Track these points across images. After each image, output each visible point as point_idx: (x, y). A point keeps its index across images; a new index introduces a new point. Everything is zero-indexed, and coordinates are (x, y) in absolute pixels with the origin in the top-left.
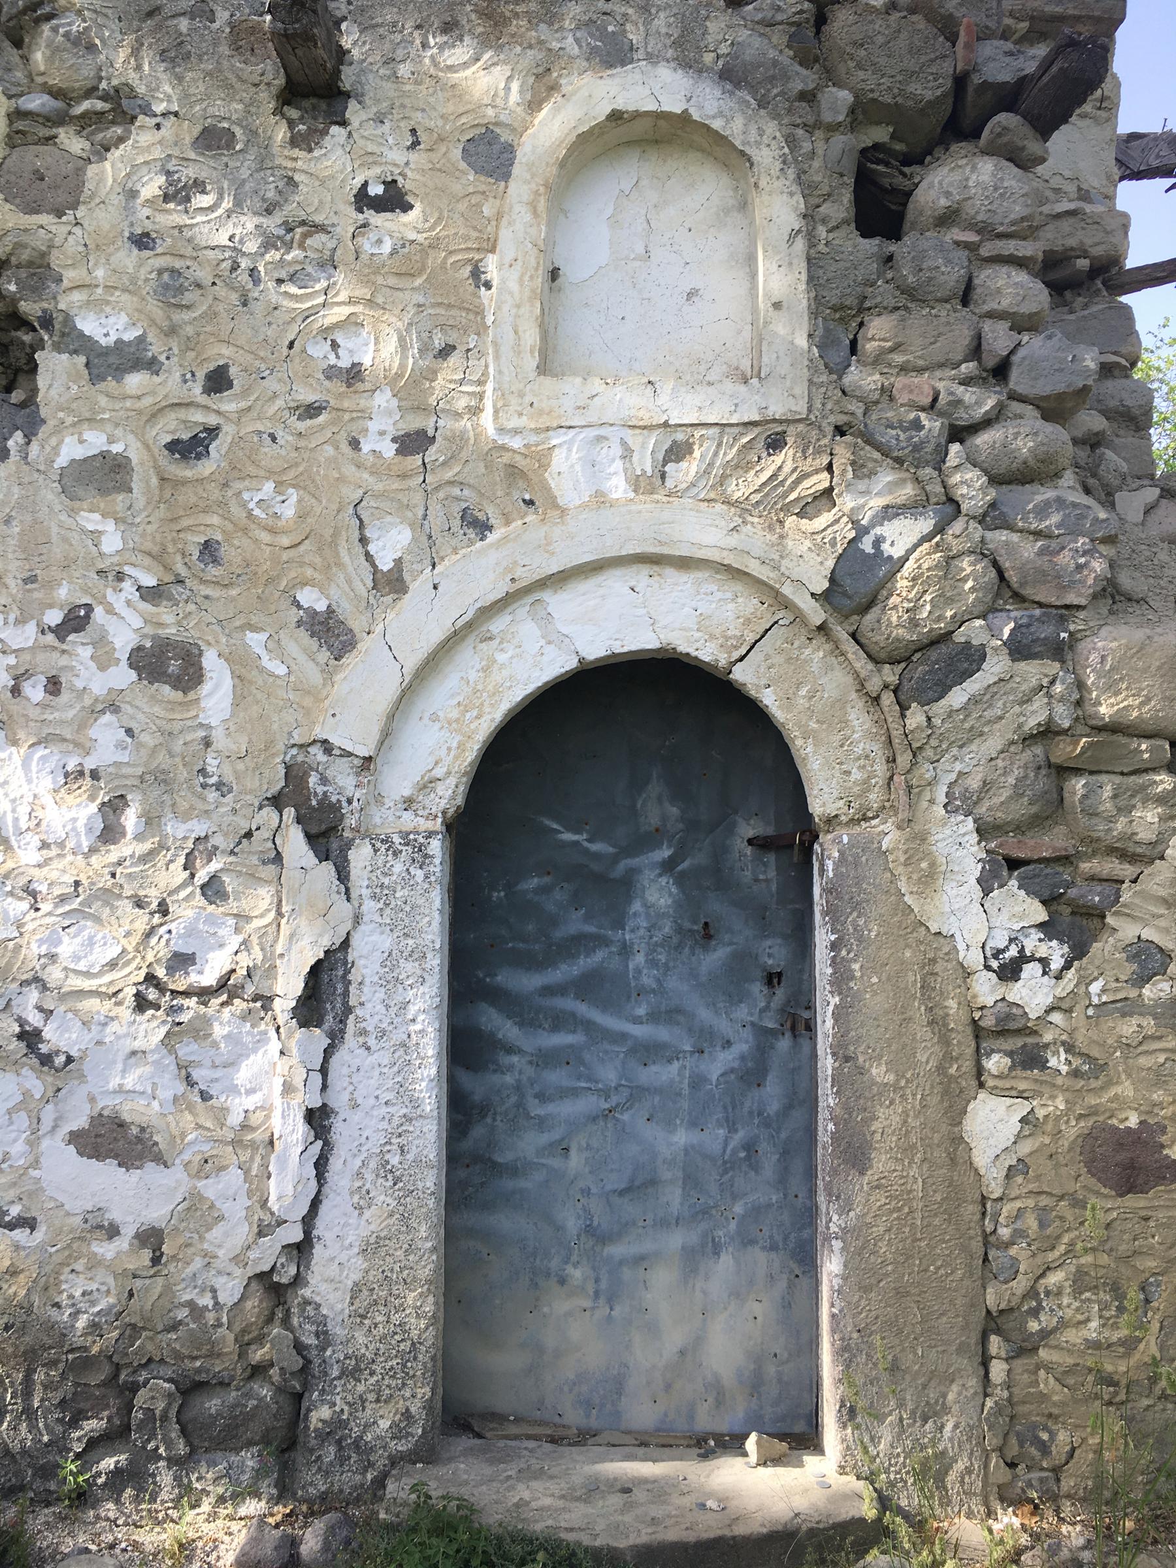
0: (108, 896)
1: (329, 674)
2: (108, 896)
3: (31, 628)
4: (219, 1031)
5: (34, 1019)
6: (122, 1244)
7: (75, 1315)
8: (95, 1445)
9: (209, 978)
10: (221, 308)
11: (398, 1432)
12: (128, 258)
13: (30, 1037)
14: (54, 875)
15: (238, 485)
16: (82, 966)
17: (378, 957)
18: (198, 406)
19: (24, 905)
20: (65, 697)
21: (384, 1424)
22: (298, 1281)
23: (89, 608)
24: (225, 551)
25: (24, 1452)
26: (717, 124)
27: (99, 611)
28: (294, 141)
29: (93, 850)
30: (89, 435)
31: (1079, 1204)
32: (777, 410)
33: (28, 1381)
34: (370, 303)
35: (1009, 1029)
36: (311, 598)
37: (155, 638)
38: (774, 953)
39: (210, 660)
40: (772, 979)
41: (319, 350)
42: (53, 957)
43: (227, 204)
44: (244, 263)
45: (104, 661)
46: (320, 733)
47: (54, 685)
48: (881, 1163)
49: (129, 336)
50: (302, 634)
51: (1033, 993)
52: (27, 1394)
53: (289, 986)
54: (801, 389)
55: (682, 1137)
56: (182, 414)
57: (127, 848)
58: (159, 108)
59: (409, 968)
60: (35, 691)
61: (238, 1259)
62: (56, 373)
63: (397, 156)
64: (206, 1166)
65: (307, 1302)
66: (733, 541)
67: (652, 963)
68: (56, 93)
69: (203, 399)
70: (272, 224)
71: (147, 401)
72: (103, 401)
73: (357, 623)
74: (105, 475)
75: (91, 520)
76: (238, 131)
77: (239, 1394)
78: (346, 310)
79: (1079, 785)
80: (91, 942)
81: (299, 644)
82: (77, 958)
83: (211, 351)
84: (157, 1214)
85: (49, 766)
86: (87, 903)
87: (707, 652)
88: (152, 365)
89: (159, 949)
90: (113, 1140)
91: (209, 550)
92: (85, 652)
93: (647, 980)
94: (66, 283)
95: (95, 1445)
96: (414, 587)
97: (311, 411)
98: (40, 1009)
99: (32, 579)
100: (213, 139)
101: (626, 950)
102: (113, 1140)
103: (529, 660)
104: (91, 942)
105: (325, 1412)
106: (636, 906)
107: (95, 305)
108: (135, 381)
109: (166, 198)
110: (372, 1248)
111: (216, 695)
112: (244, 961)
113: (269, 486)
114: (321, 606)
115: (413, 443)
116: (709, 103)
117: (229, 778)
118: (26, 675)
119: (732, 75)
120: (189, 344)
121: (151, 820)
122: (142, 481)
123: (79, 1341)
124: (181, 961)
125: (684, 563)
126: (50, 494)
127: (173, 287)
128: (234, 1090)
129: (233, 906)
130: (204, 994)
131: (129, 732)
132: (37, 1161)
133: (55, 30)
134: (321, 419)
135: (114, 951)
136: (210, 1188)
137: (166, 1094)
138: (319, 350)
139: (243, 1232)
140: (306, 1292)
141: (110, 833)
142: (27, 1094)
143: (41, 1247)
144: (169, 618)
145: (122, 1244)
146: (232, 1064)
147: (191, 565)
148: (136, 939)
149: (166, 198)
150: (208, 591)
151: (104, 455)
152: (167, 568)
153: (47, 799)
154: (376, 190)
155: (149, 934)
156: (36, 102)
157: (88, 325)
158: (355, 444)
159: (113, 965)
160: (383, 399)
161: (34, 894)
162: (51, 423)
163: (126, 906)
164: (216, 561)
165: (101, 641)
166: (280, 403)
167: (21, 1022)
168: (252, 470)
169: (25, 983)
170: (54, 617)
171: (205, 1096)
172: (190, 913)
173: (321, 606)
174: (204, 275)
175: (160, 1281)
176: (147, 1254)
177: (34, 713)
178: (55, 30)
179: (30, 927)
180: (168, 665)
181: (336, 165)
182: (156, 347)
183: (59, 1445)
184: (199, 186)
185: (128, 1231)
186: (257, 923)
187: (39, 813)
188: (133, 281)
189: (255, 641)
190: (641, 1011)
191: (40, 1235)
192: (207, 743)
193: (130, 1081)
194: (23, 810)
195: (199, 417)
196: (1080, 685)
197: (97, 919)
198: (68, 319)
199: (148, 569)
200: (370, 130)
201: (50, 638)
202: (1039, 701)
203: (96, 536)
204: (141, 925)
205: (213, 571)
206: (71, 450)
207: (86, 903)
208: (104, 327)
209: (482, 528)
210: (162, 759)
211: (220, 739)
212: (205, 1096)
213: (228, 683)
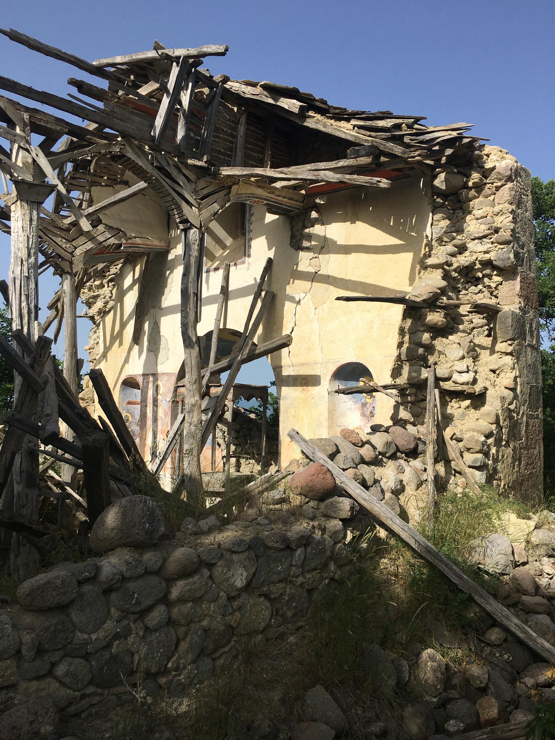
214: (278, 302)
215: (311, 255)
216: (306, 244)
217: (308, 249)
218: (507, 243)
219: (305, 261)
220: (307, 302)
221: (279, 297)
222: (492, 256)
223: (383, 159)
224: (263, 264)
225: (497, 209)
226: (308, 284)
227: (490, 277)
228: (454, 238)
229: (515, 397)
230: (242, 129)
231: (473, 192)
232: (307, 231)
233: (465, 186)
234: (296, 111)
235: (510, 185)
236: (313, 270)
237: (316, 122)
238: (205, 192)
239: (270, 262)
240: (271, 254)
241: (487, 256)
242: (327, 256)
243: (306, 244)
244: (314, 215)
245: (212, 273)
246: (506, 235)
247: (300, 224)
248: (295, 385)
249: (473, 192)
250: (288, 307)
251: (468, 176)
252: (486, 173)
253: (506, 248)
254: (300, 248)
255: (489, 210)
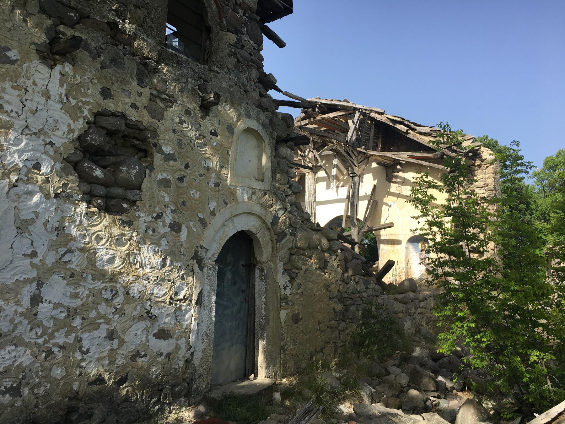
0: (163, 279)
1: (203, 231)
2: (163, 279)
3: (150, 217)
4: (183, 308)
5: (149, 308)
6: (163, 357)
7: (152, 376)
8: (155, 404)
9: (181, 297)
10: (188, 150)
11: (206, 387)
12: (172, 134)
13: (148, 312)
14: (153, 275)
15: (190, 189)
16: (158, 296)
17: (207, 291)
18: (182, 170)
19: (147, 282)
20: (156, 233)
21: (204, 386)
22: (192, 360)
23: (162, 214)
24: (187, 204)
25: (142, 410)
26: (261, 134)
27: (164, 214)
28: (201, 117)
29: (161, 269)
30: (163, 174)
31: (292, 327)
32: (266, 189)
33: (143, 392)
34: (212, 155)
35: (285, 299)
36: (201, 215)
37: (174, 222)
38: (244, 287)
39: (184, 227)
40: (243, 291)
41: (203, 162)
42: (153, 294)
43: (190, 127)
44: (193, 142)
45: (164, 226)
46: (201, 244)
47: (154, 231)
48: (271, 323)
49: (171, 152)
50: (199, 222)
51: (288, 292)
52: (142, 396)
53: (195, 298)
54: (269, 185)
55: (229, 324)
56: (180, 172)
57: (167, 268)
58: (179, 102)
59: (212, 293)
60: (150, 232)
61: (183, 357)
62: (158, 159)
63: (216, 125)
64: (178, 339)
65: (192, 364)
66: (260, 211)
67: (227, 290)
68: (158, 91)
69: (184, 169)
70: (197, 134)
71: (174, 168)
72: (166, 166)
73: (208, 221)
74: (165, 183)
75: (163, 193)
76: (192, 112)
77: (179, 386)
78: (209, 155)
79: (294, 257)
80: (160, 290)
81: (198, 224)
82: (157, 294)
83: (186, 159)
84: (170, 349)
85: (152, 249)
86: (159, 281)
87: (254, 231)
88: (175, 160)
89: (173, 291)
90: (163, 334)
91: (184, 203)
92: (161, 224)
93: (226, 293)
94: (160, 138)
95: (155, 404)
96: (217, 214)
97: (201, 175)
98: (150, 306)
99: (152, 206)
100: (188, 112)
101: (224, 288)
102: (163, 334)
103: (231, 232)
104: (160, 290)
105: (195, 386)
106: (226, 278)
107: (166, 144)
108: (172, 162)
109: (179, 123)
110: (204, 351)
111: (183, 235)
112: (188, 293)
113: (195, 190)
114: (202, 217)
115: (217, 185)
116: (260, 130)
117: (185, 253)
118: (149, 228)
119: (263, 125)
120: (182, 157)
121: (172, 263)
122: (173, 186)
123: (153, 381)
124: (176, 294)
125: (253, 214)
126: (155, 186)
127: (180, 143)
128: (184, 321)
129: (186, 281)
130: (180, 300)
131: (168, 242)
132: (148, 341)
133: (159, 76)
134: (203, 177)
135: (164, 292)
136: (180, 342)
137: (173, 323)
138: (203, 162)
139: (185, 351)
140: (193, 362)
141: (163, 265)
142: (147, 326)
143: (148, 361)
144: (177, 217)
145: (163, 357)
146: (185, 315)
147: (181, 205)
148: (168, 289)
149: (179, 123)
150: (184, 212)
151: (165, 179)
152: (177, 206)
153: (152, 257)
154: (213, 131)
155: (171, 288)
156: (155, 92)
157: (164, 148)
158: (208, 183)
159: (164, 295)
160: (213, 175)
161: (149, 279)
162: (156, 169)
163: (166, 281)
164: (185, 205)
165: (164, 221)
166: (197, 173)
167: (146, 309)
168: (191, 186)
169: (147, 300)
170: (155, 215)
171: (179, 323)
172: (179, 283)
173: (202, 217)
174: (185, 142)
175: (169, 364)
176: (168, 359)
177: (149, 237)
178: (159, 76)
179: (148, 287)
180: (175, 227)
181: (208, 124)
182: (177, 156)
183: (148, 406)
184: (185, 122)
185: (164, 354)
186: (190, 285)
187: (150, 260)
188: (173, 140)
189: (191, 223)
190: (225, 299)
191: (148, 358)
192: (182, 245)
193: (167, 320)
194: (147, 259)
195: (183, 173)
196: (296, 241)
197: (161, 285)
198: (160, 146)
199: (173, 206)
200: (213, 118)
201: (153, 220)
202: (291, 243)
203: (164, 197)
204: (169, 286)
205: (185, 208)
206: (160, 177)
207: (160, 282)
208: (167, 149)
209: (226, 204)
210: (174, 249)
211: (184, 245)
212: (179, 323)
213: (186, 232)
214: (379, 205)
215: (397, 185)
216: (394, 180)
217: (395, 182)
218: (492, 191)
219: (394, 188)
220: (394, 206)
221: (379, 203)
222: (485, 195)
223: (445, 157)
224: (372, 187)
225: (487, 176)
226: (395, 198)
227: (483, 203)
228: (469, 187)
229: (494, 253)
230: (372, 132)
231: (477, 168)
232: (395, 174)
233: (474, 165)
234: (405, 131)
235: (492, 166)
236: (398, 192)
237: (412, 135)
238: (361, 160)
239: (375, 186)
240: (375, 182)
241: (483, 195)
242: (406, 187)
243: (394, 180)
244: (399, 167)
245: (340, 188)
246: (492, 187)
247: (391, 171)
248: (387, 244)
249: (477, 168)
250: (384, 208)
251: (475, 161)
252: (482, 160)
253: (491, 193)
254: (391, 182)
255: (484, 176)
